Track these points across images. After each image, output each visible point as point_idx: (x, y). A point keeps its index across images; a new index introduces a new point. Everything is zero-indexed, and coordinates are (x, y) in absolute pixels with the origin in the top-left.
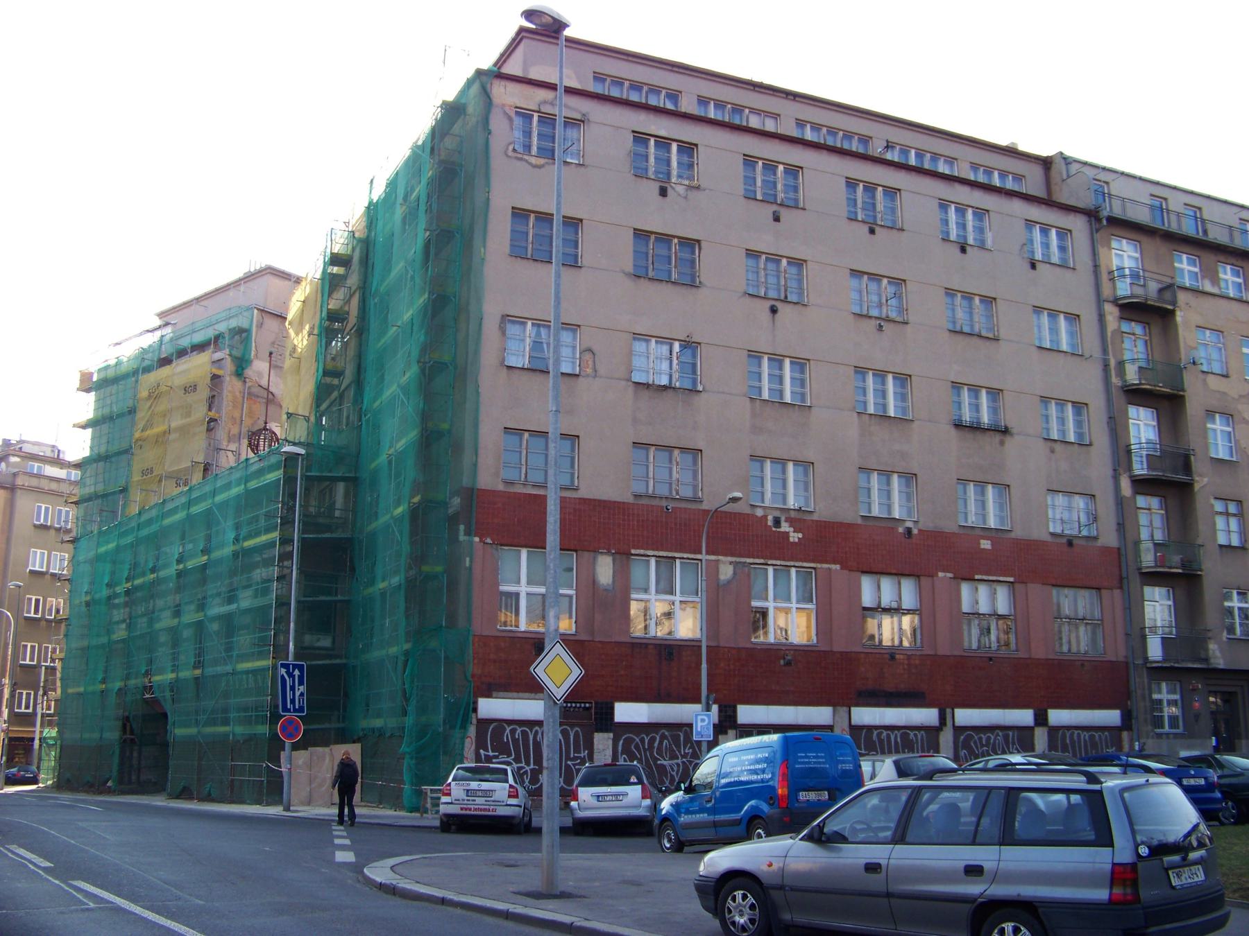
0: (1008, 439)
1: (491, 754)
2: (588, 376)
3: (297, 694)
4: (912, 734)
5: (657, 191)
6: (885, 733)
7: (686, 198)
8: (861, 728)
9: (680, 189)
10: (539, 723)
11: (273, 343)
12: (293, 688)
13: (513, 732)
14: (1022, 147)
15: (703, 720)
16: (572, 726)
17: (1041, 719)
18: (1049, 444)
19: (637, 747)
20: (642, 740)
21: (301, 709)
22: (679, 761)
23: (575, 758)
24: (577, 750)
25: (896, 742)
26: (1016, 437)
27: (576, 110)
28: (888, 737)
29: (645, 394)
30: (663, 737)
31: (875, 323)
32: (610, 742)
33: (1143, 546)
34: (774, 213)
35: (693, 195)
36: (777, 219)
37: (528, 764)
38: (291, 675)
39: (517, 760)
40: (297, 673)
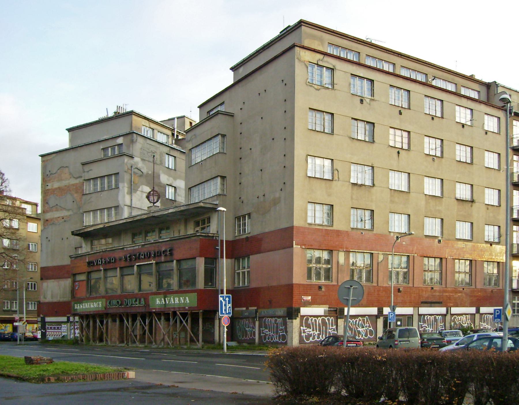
0: (474, 204)
1: (304, 328)
2: (336, 180)
3: (228, 307)
4: (437, 317)
5: (359, 102)
6: (314, 319)
7: (370, 104)
8: (421, 315)
9: (368, 100)
10: (412, 315)
11: (141, 149)
12: (225, 305)
13: (312, 320)
14: (477, 77)
15: (392, 315)
16: (331, 317)
17: (478, 311)
18: (487, 206)
19: (351, 324)
20: (353, 321)
21: (229, 313)
22: (365, 329)
23: (332, 329)
24: (332, 326)
25: (319, 324)
26: (476, 204)
27: (331, 64)
28: (315, 320)
29: (356, 188)
30: (360, 320)
31: (431, 157)
32: (343, 322)
33: (514, 245)
34: (400, 111)
35: (373, 103)
36: (400, 113)
37: (316, 331)
38: (225, 300)
39: (313, 330)
40: (227, 299)
